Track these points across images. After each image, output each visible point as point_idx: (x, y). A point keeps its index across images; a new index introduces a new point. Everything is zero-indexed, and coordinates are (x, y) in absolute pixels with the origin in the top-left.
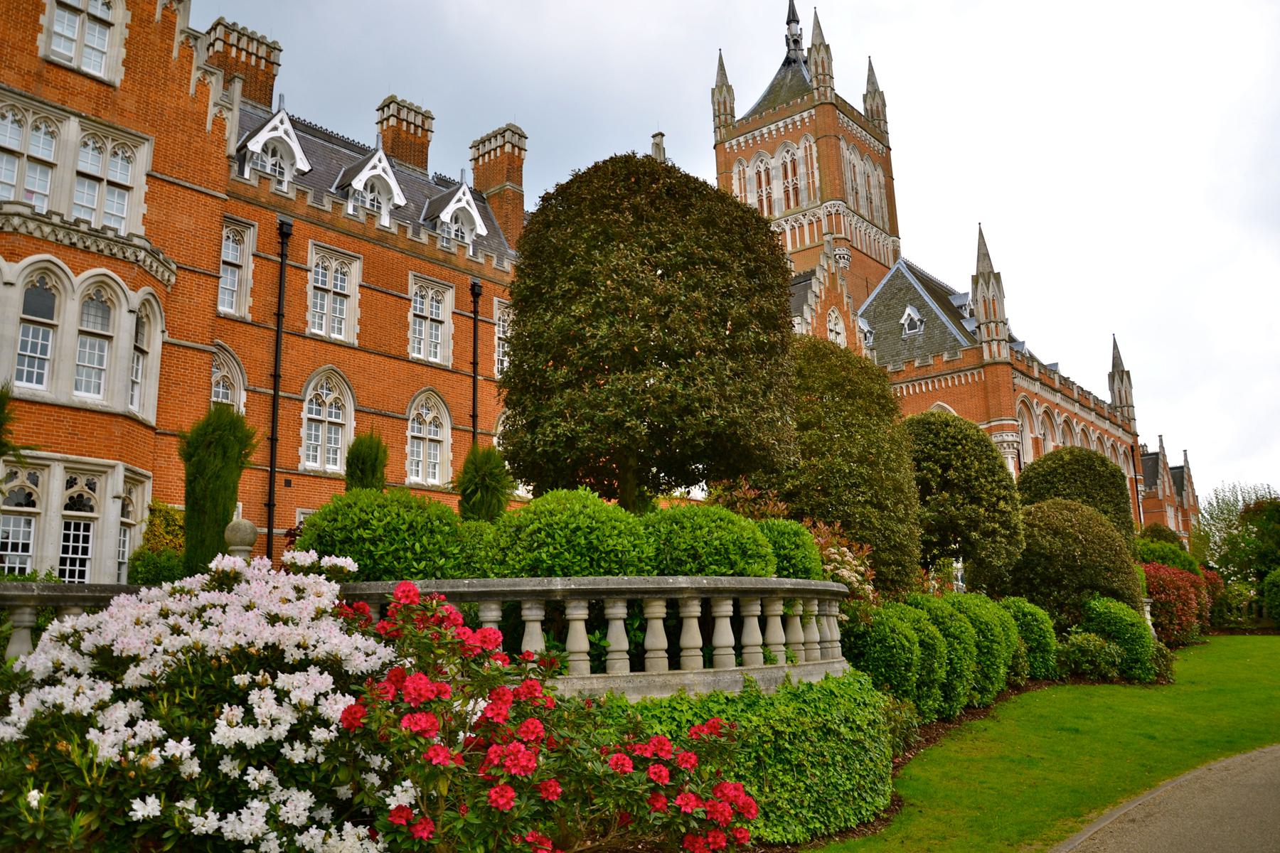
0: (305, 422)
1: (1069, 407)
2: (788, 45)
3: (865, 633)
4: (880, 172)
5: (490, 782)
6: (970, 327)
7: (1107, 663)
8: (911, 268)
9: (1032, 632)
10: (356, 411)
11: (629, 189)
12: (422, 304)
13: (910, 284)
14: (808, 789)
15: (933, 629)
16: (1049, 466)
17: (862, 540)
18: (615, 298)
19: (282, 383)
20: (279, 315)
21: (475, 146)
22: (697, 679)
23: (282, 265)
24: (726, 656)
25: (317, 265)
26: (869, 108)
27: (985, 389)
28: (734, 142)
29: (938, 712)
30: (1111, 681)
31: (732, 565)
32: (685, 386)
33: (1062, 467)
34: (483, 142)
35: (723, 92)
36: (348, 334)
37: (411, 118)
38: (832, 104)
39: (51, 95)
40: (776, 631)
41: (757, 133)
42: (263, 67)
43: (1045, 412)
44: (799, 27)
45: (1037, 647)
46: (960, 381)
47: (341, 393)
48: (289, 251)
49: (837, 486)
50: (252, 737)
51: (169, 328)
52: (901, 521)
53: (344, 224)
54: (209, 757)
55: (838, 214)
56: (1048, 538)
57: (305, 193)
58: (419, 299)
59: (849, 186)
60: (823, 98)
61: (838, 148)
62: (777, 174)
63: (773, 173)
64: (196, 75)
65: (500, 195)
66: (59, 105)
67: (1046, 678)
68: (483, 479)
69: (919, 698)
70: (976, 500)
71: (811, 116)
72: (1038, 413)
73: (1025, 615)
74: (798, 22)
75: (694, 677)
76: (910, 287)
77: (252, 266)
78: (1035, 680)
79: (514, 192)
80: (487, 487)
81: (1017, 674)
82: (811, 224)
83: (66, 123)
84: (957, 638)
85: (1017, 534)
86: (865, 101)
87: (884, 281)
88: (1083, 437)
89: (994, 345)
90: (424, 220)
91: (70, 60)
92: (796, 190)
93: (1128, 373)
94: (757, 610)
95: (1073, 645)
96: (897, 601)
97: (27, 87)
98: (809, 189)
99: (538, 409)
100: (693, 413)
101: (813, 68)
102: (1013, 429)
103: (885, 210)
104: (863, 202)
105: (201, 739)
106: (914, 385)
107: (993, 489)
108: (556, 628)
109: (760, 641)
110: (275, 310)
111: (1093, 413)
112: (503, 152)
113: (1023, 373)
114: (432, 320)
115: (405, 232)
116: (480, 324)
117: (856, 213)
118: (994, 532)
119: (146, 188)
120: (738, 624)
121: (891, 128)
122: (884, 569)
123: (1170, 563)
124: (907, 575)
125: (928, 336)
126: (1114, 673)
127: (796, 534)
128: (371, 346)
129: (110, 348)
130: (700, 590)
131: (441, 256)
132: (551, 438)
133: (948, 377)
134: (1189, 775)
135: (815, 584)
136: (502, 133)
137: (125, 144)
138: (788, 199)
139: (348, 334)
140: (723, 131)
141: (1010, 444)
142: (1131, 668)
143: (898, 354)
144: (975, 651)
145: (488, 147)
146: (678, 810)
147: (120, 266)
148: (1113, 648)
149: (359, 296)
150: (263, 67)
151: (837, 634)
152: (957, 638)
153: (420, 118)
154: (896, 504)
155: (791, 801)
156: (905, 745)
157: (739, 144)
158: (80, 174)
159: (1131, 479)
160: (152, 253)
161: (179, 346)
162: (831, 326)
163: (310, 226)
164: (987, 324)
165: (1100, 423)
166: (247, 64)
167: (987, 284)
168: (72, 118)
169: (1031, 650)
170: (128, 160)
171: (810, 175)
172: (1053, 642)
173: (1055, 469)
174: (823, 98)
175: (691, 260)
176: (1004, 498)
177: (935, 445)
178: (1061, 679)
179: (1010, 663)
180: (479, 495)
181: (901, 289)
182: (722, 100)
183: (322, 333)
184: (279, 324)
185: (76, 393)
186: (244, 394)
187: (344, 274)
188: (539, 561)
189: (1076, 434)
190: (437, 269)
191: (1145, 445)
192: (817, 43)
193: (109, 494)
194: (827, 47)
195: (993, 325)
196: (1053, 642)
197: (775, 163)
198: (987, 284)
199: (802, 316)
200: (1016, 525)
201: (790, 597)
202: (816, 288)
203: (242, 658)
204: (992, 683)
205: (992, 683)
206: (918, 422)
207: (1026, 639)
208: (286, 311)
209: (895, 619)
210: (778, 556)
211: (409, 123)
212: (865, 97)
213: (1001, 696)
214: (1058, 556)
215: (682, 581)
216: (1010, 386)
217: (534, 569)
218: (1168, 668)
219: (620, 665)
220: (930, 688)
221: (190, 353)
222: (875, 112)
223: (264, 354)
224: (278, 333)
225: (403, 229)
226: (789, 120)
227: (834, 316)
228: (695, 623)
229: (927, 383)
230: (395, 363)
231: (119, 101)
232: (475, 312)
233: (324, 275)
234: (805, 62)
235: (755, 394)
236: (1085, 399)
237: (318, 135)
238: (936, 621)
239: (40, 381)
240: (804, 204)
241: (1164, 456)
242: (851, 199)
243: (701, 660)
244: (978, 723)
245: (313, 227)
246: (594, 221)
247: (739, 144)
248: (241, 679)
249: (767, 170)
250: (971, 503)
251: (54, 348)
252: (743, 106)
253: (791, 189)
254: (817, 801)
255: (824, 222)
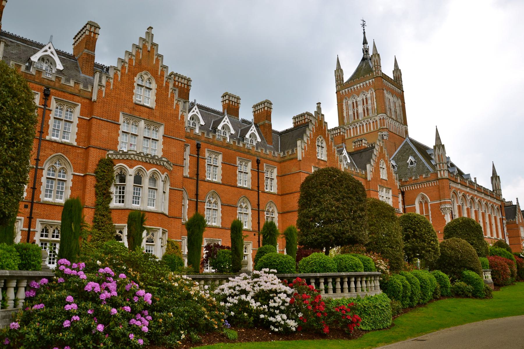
0: (206, 209)
1: (473, 193)
2: (363, 52)
3: (387, 283)
4: (400, 101)
5: (317, 312)
6: (433, 163)
7: (467, 291)
8: (412, 141)
9: (442, 281)
10: (221, 205)
11: (329, 180)
12: (241, 167)
13: (411, 147)
14: (371, 319)
15: (407, 282)
16: (454, 224)
17: (387, 257)
18: (326, 207)
19: (199, 197)
20: (197, 175)
21: (254, 107)
22: (347, 295)
23: (198, 158)
24: (353, 290)
25: (208, 157)
26: (395, 76)
27: (439, 188)
28: (344, 91)
29: (409, 305)
30: (469, 297)
31: (354, 269)
32: (343, 227)
33: (459, 224)
34: (257, 106)
35: (339, 72)
36: (218, 179)
37: (233, 100)
38: (381, 77)
39: (137, 114)
40: (364, 284)
41: (352, 88)
42: (186, 87)
43: (463, 195)
44: (368, 45)
45: (444, 286)
46: (429, 185)
47: (217, 199)
48: (200, 153)
49: (380, 242)
50: (276, 305)
51: (171, 185)
52: (398, 251)
53: (216, 142)
54: (269, 308)
55: (383, 119)
56: (450, 251)
57: (204, 133)
58: (240, 166)
59: (388, 107)
60: (377, 74)
61: (383, 93)
62: (360, 103)
63: (358, 103)
64: (175, 102)
65: (264, 125)
66: (138, 117)
67: (447, 296)
68: (270, 232)
69: (403, 300)
70: (424, 241)
71: (373, 81)
72: (460, 196)
73: (440, 276)
74: (367, 44)
75: (346, 294)
76: (411, 149)
77: (189, 159)
78: (443, 296)
79: (268, 124)
80: (271, 234)
81: (437, 294)
82: (373, 122)
83: (140, 122)
84: (414, 284)
85: (437, 251)
86: (393, 73)
87: (401, 146)
88: (479, 204)
89: (442, 171)
90: (240, 137)
91: (140, 102)
92: (367, 109)
93: (499, 177)
94: (360, 279)
95: (456, 285)
96: (397, 274)
97: (130, 113)
98: (372, 109)
99: (308, 232)
100: (344, 234)
101: (373, 63)
102: (449, 203)
103: (402, 115)
104: (393, 113)
105: (268, 305)
106: (412, 187)
107: (429, 237)
108: (318, 284)
109: (360, 286)
110: (196, 173)
111: (483, 194)
112: (264, 110)
113: (453, 181)
114: (244, 173)
115: (235, 143)
116: (260, 173)
117: (390, 118)
118: (430, 250)
119: (162, 140)
120: (355, 283)
121: (404, 83)
122: (393, 265)
123: (503, 256)
124: (400, 266)
125: (418, 167)
126: (470, 295)
127: (369, 260)
128: (225, 183)
129: (157, 192)
130: (348, 276)
131: (247, 151)
132: (311, 239)
133: (425, 184)
134: (475, 323)
135: (373, 273)
136: (264, 103)
137: (156, 125)
138: (364, 113)
139: (218, 179)
140: (339, 87)
141: (448, 209)
142: (476, 293)
143: (406, 174)
144: (420, 288)
145: (259, 108)
146: (347, 318)
147: (159, 167)
148: (470, 287)
149: (221, 166)
150: (186, 87)
151: (378, 284)
152: (414, 284)
153: (236, 99)
154: (397, 246)
155: (367, 321)
156: (396, 313)
157: (345, 92)
158: (144, 137)
159: (500, 219)
160: (167, 162)
161: (173, 189)
162: (381, 166)
163: (206, 144)
164: (439, 164)
165: (486, 198)
166: (181, 87)
167: (439, 149)
168: (142, 120)
169: (441, 287)
170: (157, 131)
171: (373, 104)
172: (449, 285)
173: (457, 225)
174: (377, 74)
175: (344, 197)
176: (433, 240)
177: (411, 224)
178: (452, 296)
179: (434, 291)
180: (269, 237)
181: (408, 149)
182: (339, 75)
183: (210, 179)
184: (197, 177)
185: (148, 207)
186: (187, 201)
187: (216, 159)
188: (313, 269)
189: (476, 203)
190: (246, 155)
191: (511, 201)
192: (375, 53)
193: (158, 238)
194: (379, 55)
195: (441, 164)
196: (449, 285)
197: (359, 99)
198: (439, 149)
199: (370, 163)
200: (437, 248)
201: (367, 276)
202: (375, 153)
203: (271, 291)
204: (427, 297)
205: (427, 297)
206: (406, 216)
207: (440, 284)
208: (199, 173)
209: (396, 279)
210: (364, 266)
211: (232, 102)
212: (393, 72)
213: (431, 301)
214: (453, 257)
215: (344, 274)
216: (448, 187)
217: (312, 271)
218: (490, 293)
219: (331, 292)
220: (406, 298)
221: (176, 191)
222: (397, 78)
223: (193, 188)
224: (197, 180)
225: (234, 142)
226: (364, 83)
227: (382, 162)
228: (346, 283)
229: (417, 186)
230: (233, 188)
231: (155, 113)
232: (258, 169)
233: (210, 160)
234: (370, 59)
235: (358, 228)
236: (480, 189)
237: (204, 109)
238: (408, 279)
239: (138, 204)
240: (371, 115)
241: (519, 206)
242: (388, 113)
243: (348, 291)
244: (421, 308)
245: (207, 144)
246: (321, 188)
247: (345, 92)
248: (271, 295)
249: (356, 102)
250: (422, 242)
251: (142, 193)
252: (346, 78)
253: (365, 109)
254: (373, 322)
255: (378, 122)
